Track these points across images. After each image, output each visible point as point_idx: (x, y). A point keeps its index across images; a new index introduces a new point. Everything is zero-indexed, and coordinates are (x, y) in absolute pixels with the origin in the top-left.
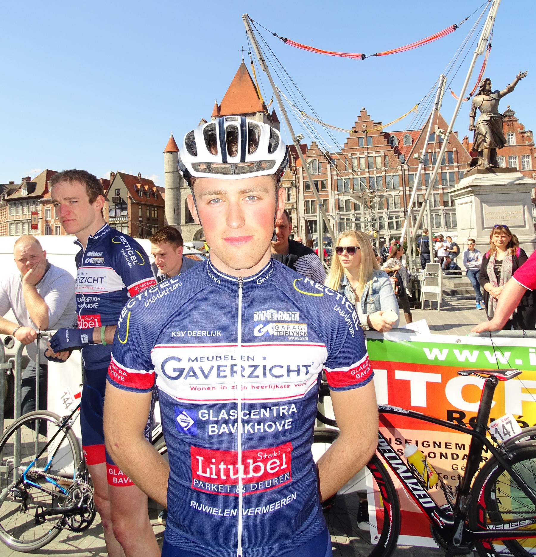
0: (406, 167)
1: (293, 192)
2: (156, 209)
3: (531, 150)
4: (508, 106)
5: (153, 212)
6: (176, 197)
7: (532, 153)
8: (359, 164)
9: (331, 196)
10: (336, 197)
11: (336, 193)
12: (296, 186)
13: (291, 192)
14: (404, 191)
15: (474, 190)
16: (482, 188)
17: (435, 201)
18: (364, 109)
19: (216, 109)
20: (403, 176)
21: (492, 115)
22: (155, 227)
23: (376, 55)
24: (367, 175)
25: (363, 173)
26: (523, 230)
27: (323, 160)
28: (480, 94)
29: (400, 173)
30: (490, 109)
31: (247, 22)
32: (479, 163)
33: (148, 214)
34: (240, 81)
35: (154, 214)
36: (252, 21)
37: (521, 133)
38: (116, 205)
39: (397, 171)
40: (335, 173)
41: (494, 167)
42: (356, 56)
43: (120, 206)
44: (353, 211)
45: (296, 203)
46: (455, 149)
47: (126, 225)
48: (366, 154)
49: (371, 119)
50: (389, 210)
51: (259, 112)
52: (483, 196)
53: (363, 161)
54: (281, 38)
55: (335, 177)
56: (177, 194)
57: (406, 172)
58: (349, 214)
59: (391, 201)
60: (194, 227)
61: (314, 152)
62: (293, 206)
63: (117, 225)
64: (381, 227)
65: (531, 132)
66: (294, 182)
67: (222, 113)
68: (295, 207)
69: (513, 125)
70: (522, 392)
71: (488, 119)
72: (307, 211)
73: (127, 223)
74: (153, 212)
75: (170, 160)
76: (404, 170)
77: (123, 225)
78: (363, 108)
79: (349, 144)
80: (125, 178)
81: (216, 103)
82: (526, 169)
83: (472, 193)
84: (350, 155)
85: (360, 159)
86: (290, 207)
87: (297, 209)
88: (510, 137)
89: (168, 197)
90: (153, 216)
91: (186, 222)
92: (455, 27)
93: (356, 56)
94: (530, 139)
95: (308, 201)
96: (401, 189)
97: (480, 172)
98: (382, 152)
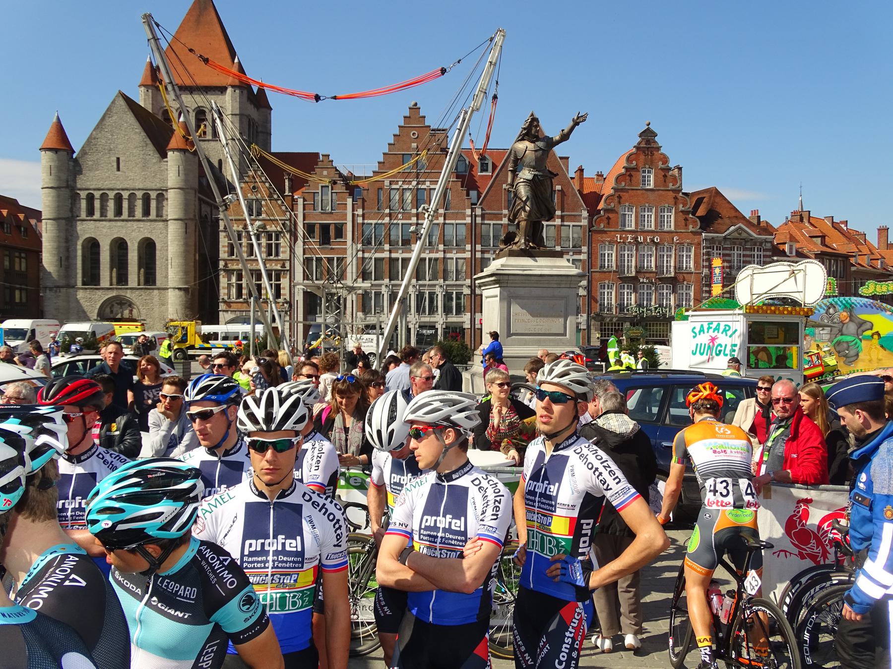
0: (478, 212)
2: (23, 255)
3: (676, 198)
4: (647, 122)
5: (17, 260)
7: (676, 204)
8: (402, 200)
9: (351, 250)
10: (360, 254)
12: (290, 231)
13: (281, 241)
14: (473, 251)
15: (500, 279)
16: (511, 278)
18: (416, 104)
19: (149, 73)
20: (473, 227)
21: (536, 173)
22: (21, 290)
23: (335, 98)
26: (561, 340)
27: (340, 187)
28: (522, 139)
30: (533, 164)
31: (150, 26)
32: (517, 240)
33: (7, 263)
34: (198, 22)
35: (21, 265)
36: (158, 25)
37: (662, 169)
39: (464, 217)
40: (360, 212)
41: (536, 247)
42: (307, 96)
44: (387, 281)
45: (290, 260)
49: (426, 124)
50: (447, 282)
51: (233, 86)
52: (512, 290)
53: (408, 196)
54: (201, 56)
55: (360, 220)
56: (67, 230)
57: (479, 220)
58: (381, 285)
59: (452, 266)
60: (99, 293)
62: (283, 266)
64: (433, 310)
65: (680, 169)
66: (288, 222)
68: (288, 268)
69: (652, 154)
70: (247, 504)
71: (530, 177)
74: (17, 260)
75: (52, 164)
76: (476, 216)
78: (413, 103)
79: (387, 165)
81: (148, 60)
82: (666, 229)
83: (497, 283)
84: (387, 183)
86: (279, 267)
87: (290, 270)
88: (646, 174)
89: (48, 233)
90: (17, 268)
91: (84, 284)
92: (443, 71)
93: (307, 96)
94: (675, 180)
95: (312, 259)
96: (468, 247)
97: (512, 254)
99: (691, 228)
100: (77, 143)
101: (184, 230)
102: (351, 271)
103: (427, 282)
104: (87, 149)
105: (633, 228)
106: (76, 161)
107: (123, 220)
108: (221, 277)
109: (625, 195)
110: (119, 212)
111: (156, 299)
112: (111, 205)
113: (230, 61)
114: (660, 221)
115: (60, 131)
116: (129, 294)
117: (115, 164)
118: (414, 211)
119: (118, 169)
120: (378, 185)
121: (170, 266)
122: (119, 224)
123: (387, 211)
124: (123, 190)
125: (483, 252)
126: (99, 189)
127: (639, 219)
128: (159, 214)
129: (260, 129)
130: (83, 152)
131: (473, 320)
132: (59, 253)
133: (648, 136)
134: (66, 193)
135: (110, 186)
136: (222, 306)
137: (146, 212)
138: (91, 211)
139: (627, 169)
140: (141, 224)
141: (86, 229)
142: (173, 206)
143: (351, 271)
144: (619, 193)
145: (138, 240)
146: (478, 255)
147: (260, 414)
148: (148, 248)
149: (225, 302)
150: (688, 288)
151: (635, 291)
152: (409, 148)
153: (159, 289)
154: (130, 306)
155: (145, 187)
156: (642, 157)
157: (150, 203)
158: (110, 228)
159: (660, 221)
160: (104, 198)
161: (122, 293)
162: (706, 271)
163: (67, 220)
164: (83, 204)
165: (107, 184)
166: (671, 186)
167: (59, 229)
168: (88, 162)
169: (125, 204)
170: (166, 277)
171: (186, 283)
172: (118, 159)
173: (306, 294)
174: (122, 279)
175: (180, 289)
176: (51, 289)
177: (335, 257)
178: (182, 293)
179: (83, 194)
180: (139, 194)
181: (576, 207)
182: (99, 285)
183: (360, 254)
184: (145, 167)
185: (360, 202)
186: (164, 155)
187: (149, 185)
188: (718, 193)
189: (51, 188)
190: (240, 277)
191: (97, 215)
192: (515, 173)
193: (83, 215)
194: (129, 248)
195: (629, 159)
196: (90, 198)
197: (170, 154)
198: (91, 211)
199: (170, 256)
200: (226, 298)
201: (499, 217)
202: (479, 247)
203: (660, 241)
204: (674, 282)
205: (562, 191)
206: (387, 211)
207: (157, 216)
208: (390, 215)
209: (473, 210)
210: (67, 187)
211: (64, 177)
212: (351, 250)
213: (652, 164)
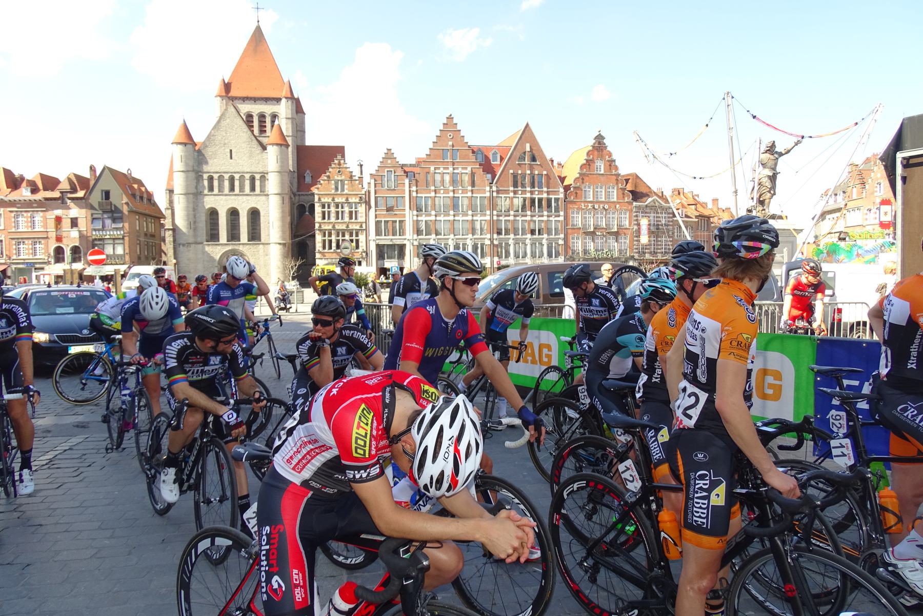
0: (494, 188)
1: (362, 209)
6: (191, 205)
8: (443, 181)
10: (415, 218)
11: (415, 213)
12: (366, 202)
14: (492, 215)
17: (481, 228)
20: (491, 199)
24: (451, 194)
25: (446, 191)
27: (400, 172)
29: (488, 194)
34: (255, 51)
38: (104, 212)
43: (110, 215)
46: (545, 173)
47: (121, 241)
48: (451, 169)
53: (447, 178)
55: (414, 194)
57: (495, 194)
59: (478, 226)
60: (219, 247)
61: (389, 161)
62: (361, 226)
63: (106, 242)
67: (233, 93)
72: (378, 233)
73: (123, 239)
77: (117, 241)
80: (115, 174)
84: (432, 168)
85: (443, 174)
86: (358, 227)
98: (469, 169)
99: (626, 200)
100: (199, 137)
102: (409, 227)
103: (461, 237)
104: (207, 143)
105: (591, 199)
106: (199, 151)
109: (586, 179)
110: (232, 189)
111: (261, 251)
112: (227, 184)
114: (608, 195)
116: (241, 248)
118: (451, 188)
119: (231, 158)
120: (427, 170)
123: (433, 188)
125: (498, 216)
127: (595, 194)
131: (157, 325)
132: (188, 220)
133: (600, 139)
134: (192, 175)
135: (238, 170)
136: (318, 255)
137: (253, 189)
139: (587, 161)
140: (249, 198)
141: (210, 202)
142: (273, 184)
143: (409, 227)
144: (582, 177)
146: (495, 218)
147: (522, 287)
148: (254, 214)
149: (320, 252)
150: (625, 239)
151: (593, 240)
152: (447, 145)
156: (596, 153)
157: (255, 182)
158: (226, 200)
159: (608, 195)
160: (221, 178)
161: (236, 247)
162: (636, 227)
163: (195, 195)
164: (206, 183)
165: (223, 169)
166: (614, 172)
167: (188, 201)
168: (208, 153)
169: (237, 183)
171: (284, 239)
173: (378, 246)
174: (234, 235)
175: (280, 244)
176: (184, 245)
177: (398, 220)
178: (281, 247)
179: (205, 176)
180: (247, 176)
181: (556, 186)
182: (239, 240)
183: (415, 218)
184: (251, 157)
185: (414, 182)
187: (254, 170)
188: (637, 176)
190: (330, 235)
191: (216, 191)
193: (206, 192)
195: (588, 154)
196: (211, 179)
198: (211, 189)
201: (507, 192)
202: (495, 213)
203: (608, 207)
204: (617, 234)
205: (547, 175)
206: (433, 188)
208: (435, 191)
209: (491, 187)
210: (193, 171)
211: (191, 163)
212: (409, 217)
213: (602, 157)
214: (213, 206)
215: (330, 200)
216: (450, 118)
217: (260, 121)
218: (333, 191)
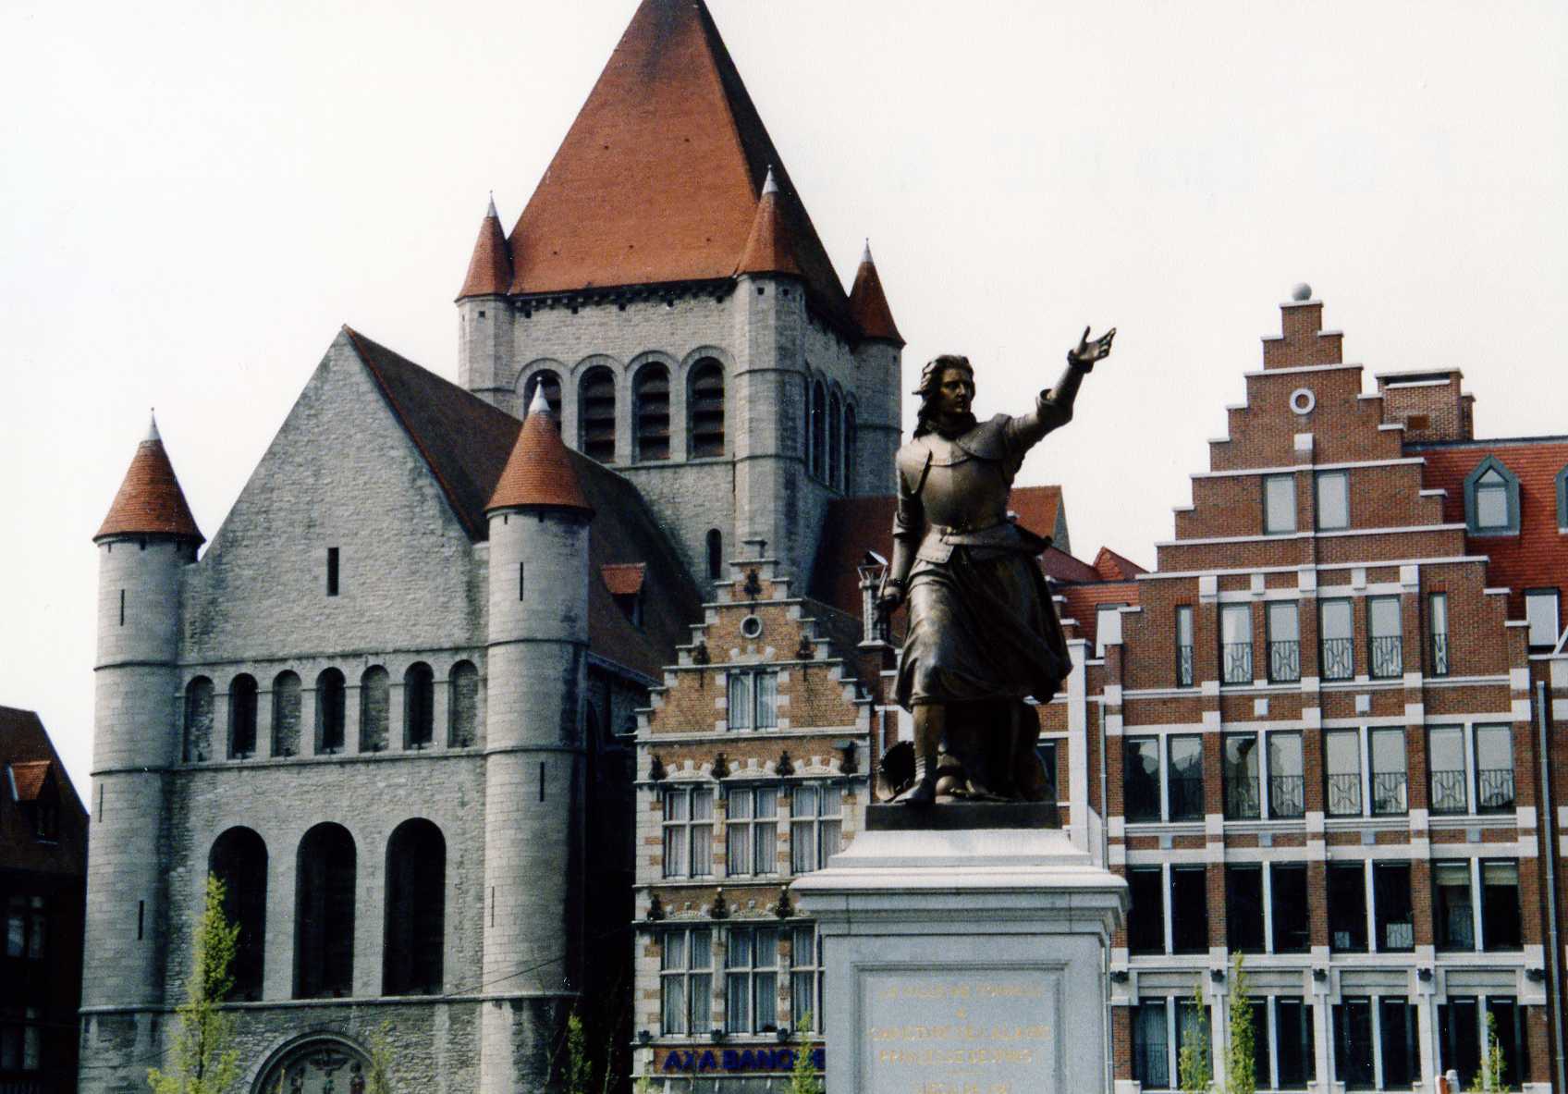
8: (1263, 648)
39: (1502, 697)
48: (1307, 581)
51: (755, 276)
67: (540, 278)
98: (1409, 573)
100: (209, 516)
101: (536, 788)
107: (342, 763)
108: (639, 952)
112: (309, 713)
113: (746, 189)
115: (156, 469)
117: (323, 572)
119: (333, 588)
120: (1180, 592)
121: (487, 920)
122: (332, 775)
124: (345, 656)
126: (271, 661)
128: (459, 737)
129: (863, 416)
130: (228, 537)
135: (307, 648)
137: (419, 729)
138: (242, 739)
141: (224, 801)
142: (506, 706)
145: (388, 831)
148: (418, 850)
153: (450, 1002)
154: (357, 1068)
155: (414, 645)
157: (430, 699)
161: (326, 1015)
163: (168, 779)
170: (478, 960)
171: (541, 979)
172: (334, 554)
174: (324, 962)
175: (517, 1003)
186: (478, 532)
187: (425, 637)
189: (558, 641)
192: (913, 541)
193: (218, 748)
194: (359, 861)
197: (496, 524)
198: (242, 739)
199: (489, 882)
200: (655, 1029)
207: (363, 748)
214: (317, 820)
215: (705, 773)
216: (1303, 313)
217: (641, 399)
218: (720, 730)
